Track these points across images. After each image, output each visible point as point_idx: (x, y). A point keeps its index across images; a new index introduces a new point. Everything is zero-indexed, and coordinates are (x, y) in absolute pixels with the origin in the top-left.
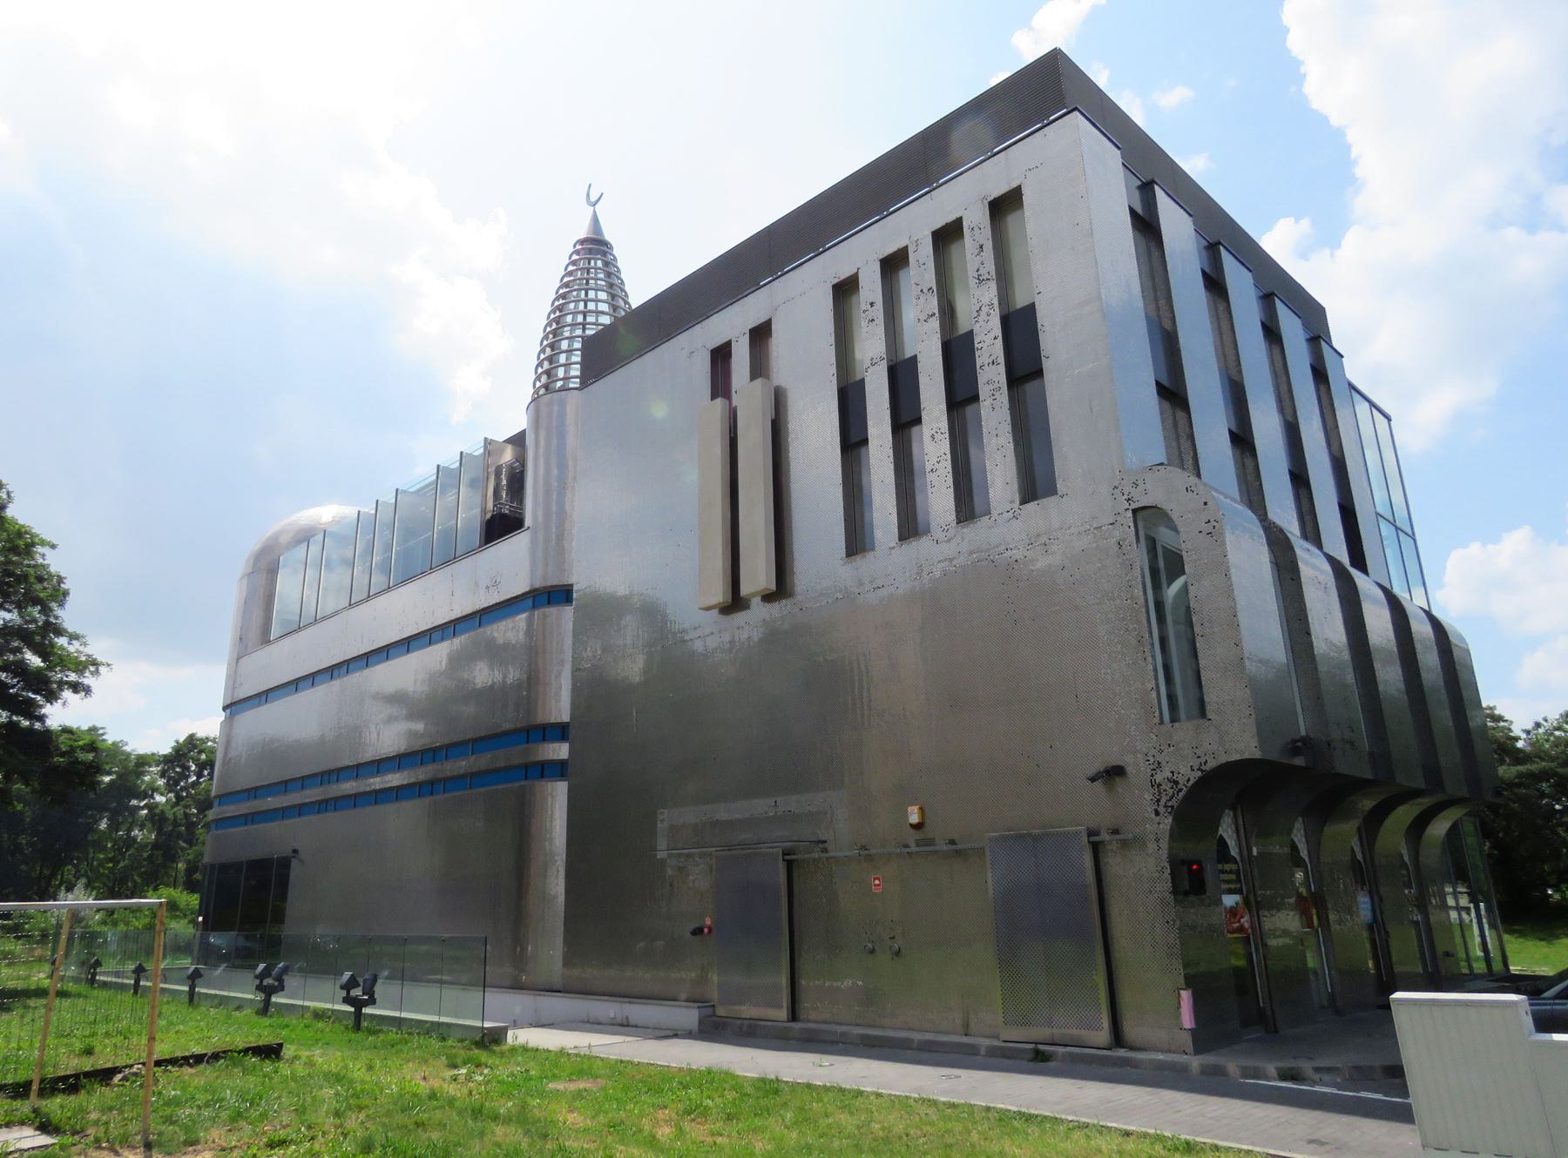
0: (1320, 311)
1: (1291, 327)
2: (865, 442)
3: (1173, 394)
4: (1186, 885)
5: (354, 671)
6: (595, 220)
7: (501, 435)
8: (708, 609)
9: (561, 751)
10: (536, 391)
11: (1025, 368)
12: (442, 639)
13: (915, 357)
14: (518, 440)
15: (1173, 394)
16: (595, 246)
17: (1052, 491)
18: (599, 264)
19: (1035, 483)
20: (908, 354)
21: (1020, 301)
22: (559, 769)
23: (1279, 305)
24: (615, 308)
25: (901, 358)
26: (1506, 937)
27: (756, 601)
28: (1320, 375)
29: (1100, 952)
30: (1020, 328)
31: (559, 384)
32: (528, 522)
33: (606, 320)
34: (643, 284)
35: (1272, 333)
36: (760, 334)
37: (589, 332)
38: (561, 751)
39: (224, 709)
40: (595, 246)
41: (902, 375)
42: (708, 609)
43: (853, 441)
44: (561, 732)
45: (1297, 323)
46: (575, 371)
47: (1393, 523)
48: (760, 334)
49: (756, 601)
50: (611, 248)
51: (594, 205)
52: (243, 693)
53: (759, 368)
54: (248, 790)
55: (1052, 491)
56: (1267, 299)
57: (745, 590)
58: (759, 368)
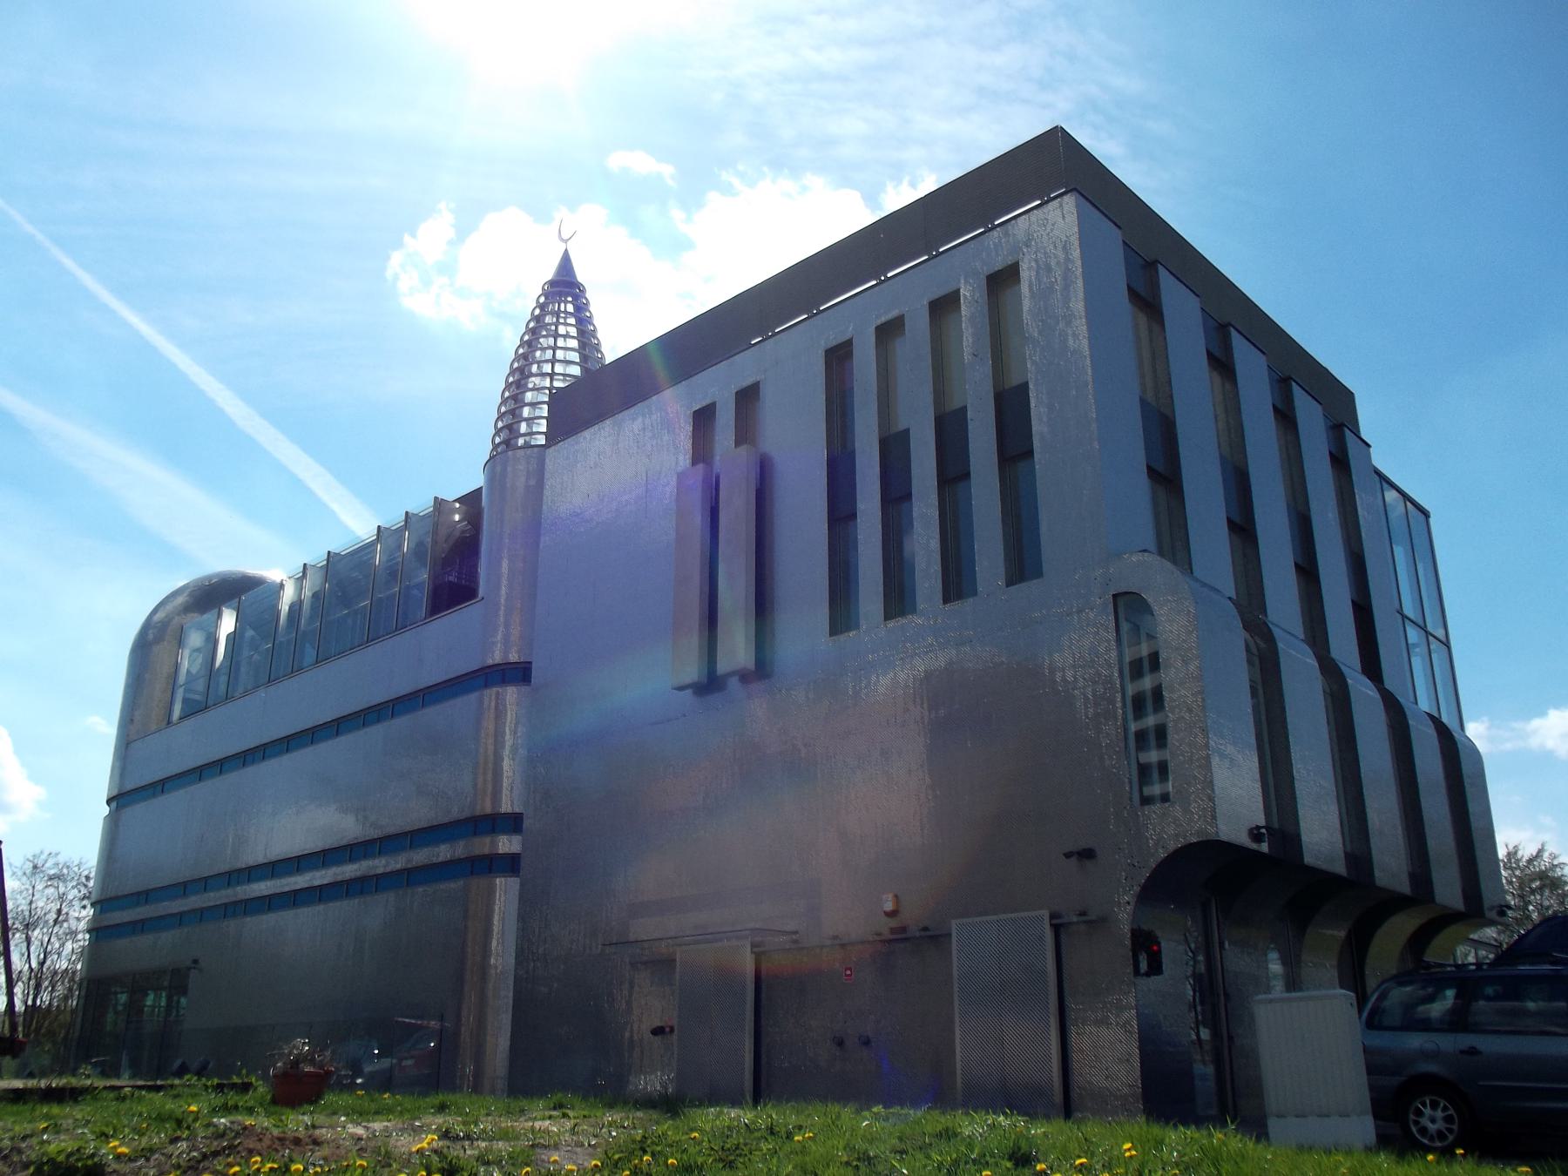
0: (1348, 397)
1: (1309, 414)
2: (853, 516)
3: (1165, 476)
4: (1144, 966)
5: (271, 757)
6: (566, 253)
7: (452, 492)
8: (681, 688)
9: (507, 844)
10: (495, 447)
11: (1015, 446)
12: (378, 721)
13: (907, 431)
14: (471, 500)
15: (1165, 476)
16: (564, 286)
17: (1038, 573)
18: (570, 308)
19: (1022, 563)
20: (901, 427)
21: (1014, 380)
22: (511, 864)
23: (1297, 391)
24: (584, 358)
25: (894, 430)
26: (673, 406)
27: (734, 682)
28: (1340, 462)
29: (1053, 1022)
30: (1011, 407)
31: (521, 442)
32: (481, 592)
33: (575, 370)
34: (622, 332)
35: (1285, 416)
36: (748, 397)
37: (557, 384)
38: (507, 844)
39: (109, 802)
40: (564, 286)
41: (894, 448)
42: (681, 688)
43: (841, 514)
44: (513, 823)
45: (1317, 410)
46: (542, 426)
47: (1424, 628)
48: (748, 397)
49: (734, 682)
50: (583, 291)
51: (566, 241)
52: (129, 786)
53: (745, 431)
54: (138, 894)
55: (1038, 573)
56: (1282, 385)
57: (722, 667)
58: (745, 431)
